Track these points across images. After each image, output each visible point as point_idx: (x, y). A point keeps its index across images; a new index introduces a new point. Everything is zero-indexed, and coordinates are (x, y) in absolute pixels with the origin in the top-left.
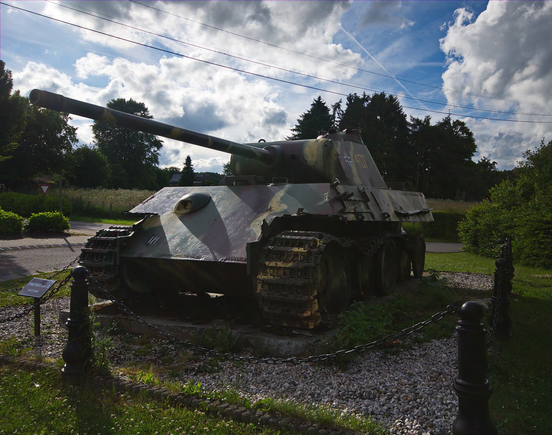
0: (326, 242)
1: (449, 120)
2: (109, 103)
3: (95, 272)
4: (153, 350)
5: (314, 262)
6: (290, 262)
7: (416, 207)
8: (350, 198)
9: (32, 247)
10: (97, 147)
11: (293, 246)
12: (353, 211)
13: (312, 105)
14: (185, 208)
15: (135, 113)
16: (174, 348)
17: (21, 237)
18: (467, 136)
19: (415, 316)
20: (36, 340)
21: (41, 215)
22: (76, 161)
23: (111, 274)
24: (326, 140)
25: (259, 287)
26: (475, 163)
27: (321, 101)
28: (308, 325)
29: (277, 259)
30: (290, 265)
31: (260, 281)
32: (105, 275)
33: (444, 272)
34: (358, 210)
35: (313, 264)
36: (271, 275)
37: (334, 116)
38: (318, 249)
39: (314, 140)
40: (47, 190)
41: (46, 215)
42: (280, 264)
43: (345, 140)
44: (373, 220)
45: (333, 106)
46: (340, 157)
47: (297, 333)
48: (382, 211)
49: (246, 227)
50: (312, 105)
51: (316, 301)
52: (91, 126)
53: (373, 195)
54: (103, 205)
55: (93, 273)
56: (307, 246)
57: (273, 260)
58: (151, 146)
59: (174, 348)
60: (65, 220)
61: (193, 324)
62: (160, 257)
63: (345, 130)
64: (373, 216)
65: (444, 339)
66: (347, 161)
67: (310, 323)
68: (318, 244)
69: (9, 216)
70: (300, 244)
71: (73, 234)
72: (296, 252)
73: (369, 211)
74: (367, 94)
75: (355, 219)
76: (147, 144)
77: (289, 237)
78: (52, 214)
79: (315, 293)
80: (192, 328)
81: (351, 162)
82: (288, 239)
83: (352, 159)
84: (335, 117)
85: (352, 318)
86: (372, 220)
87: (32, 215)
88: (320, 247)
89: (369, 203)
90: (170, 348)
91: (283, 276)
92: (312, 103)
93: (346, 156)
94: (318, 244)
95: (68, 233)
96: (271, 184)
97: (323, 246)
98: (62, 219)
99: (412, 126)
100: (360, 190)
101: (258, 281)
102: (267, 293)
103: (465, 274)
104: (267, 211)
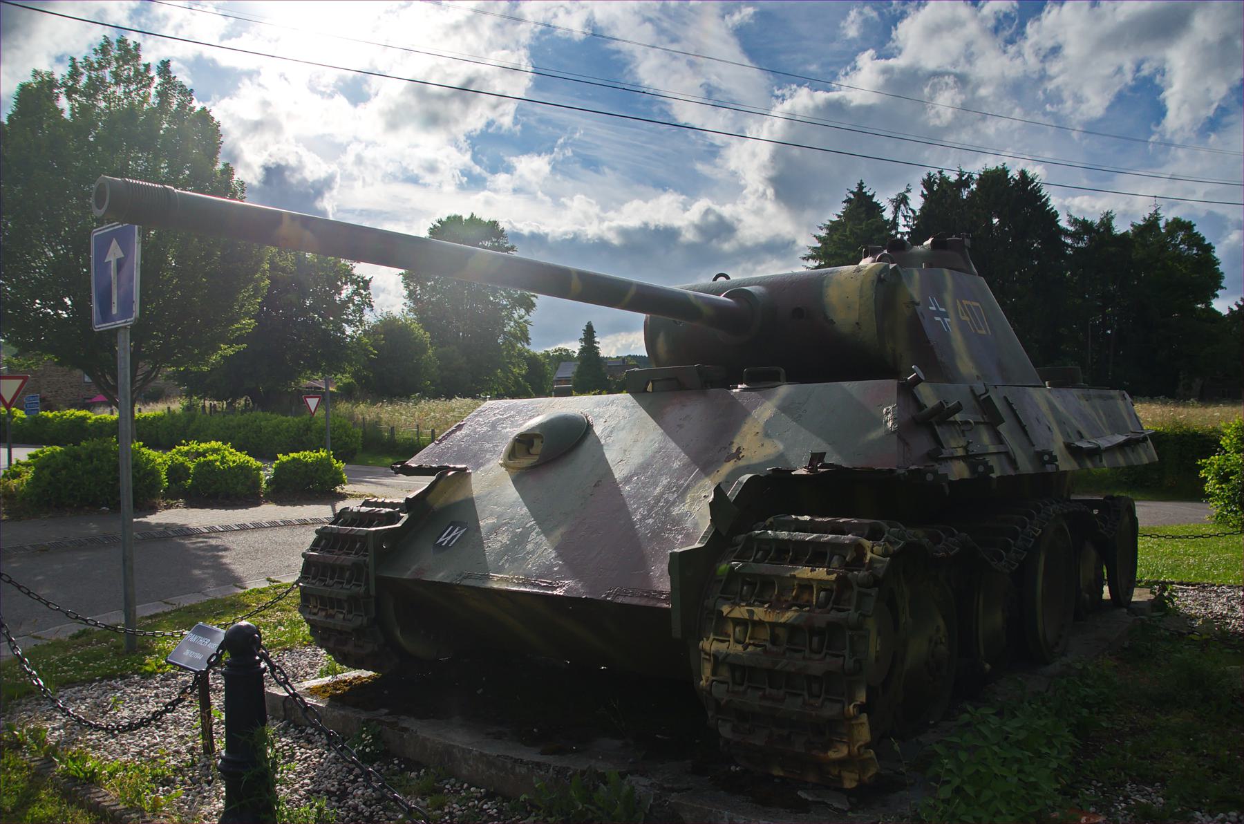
0: (891, 549)
1: (1158, 219)
2: (432, 227)
3: (330, 608)
4: (447, 814)
5: (856, 611)
6: (788, 608)
7: (1116, 428)
8: (952, 419)
9: (274, 525)
10: (412, 316)
11: (795, 561)
12: (960, 452)
13: (845, 202)
14: (530, 453)
15: (480, 243)
16: (495, 810)
17: (257, 503)
18: (1200, 252)
19: (1131, 728)
20: (203, 766)
21: (293, 457)
22: (371, 349)
23: (362, 616)
24: (882, 266)
25: (707, 670)
26: (1220, 314)
27: (864, 191)
28: (840, 778)
29: (754, 598)
30: (789, 616)
31: (707, 657)
32: (350, 616)
33: (1181, 583)
34: (975, 449)
35: (853, 615)
36: (737, 641)
37: (894, 224)
38: (866, 573)
39: (852, 268)
40: (317, 406)
41: (302, 458)
42: (760, 613)
43: (930, 265)
44: (1013, 474)
45: (892, 201)
46: (919, 309)
47: (810, 799)
48: (1033, 445)
49: (673, 503)
50: (845, 202)
51: (864, 718)
52: (400, 274)
53: (1010, 405)
54: (418, 431)
55: (327, 610)
56: (835, 562)
57: (743, 601)
58: (514, 307)
59: (495, 810)
60: (336, 468)
61: (543, 753)
62: (461, 580)
63: (929, 241)
64: (1013, 462)
65: (1231, 813)
66: (937, 319)
67: (845, 774)
68: (868, 558)
69: (238, 461)
70: (817, 555)
71: (352, 495)
72: (803, 579)
73: (1002, 449)
74: (967, 169)
75: (966, 474)
76: (505, 303)
77: (784, 534)
78: (312, 455)
79: (862, 697)
80: (538, 765)
81: (949, 320)
82: (783, 540)
83: (952, 313)
84: (898, 224)
85: (963, 756)
86: (1011, 472)
87: (277, 459)
88: (875, 565)
89: (1002, 428)
90: (486, 810)
91: (769, 645)
92: (845, 198)
93: (936, 306)
94: (868, 558)
95: (342, 493)
96: (739, 386)
97: (881, 562)
98: (331, 465)
99: (1071, 235)
100: (978, 394)
101: (703, 655)
102: (728, 691)
103: (1236, 590)
104: (728, 460)
